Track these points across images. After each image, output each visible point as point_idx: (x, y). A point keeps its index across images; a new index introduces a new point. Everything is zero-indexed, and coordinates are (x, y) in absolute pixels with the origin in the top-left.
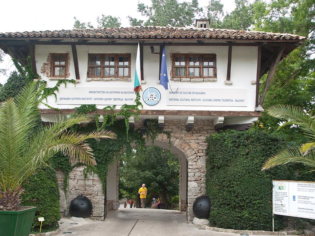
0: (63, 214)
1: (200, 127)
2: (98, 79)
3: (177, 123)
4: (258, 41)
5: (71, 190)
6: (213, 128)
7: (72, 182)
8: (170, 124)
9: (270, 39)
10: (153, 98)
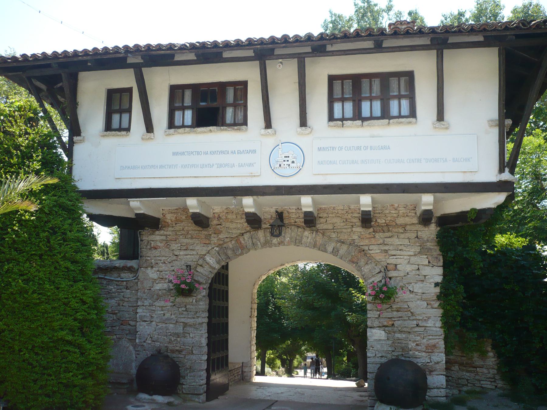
0: (126, 387)
1: (389, 218)
2: (186, 131)
3: (344, 212)
4: (494, 33)
5: (144, 342)
6: (415, 220)
7: (147, 327)
8: (330, 215)
9: (521, 29)
10: (290, 163)
